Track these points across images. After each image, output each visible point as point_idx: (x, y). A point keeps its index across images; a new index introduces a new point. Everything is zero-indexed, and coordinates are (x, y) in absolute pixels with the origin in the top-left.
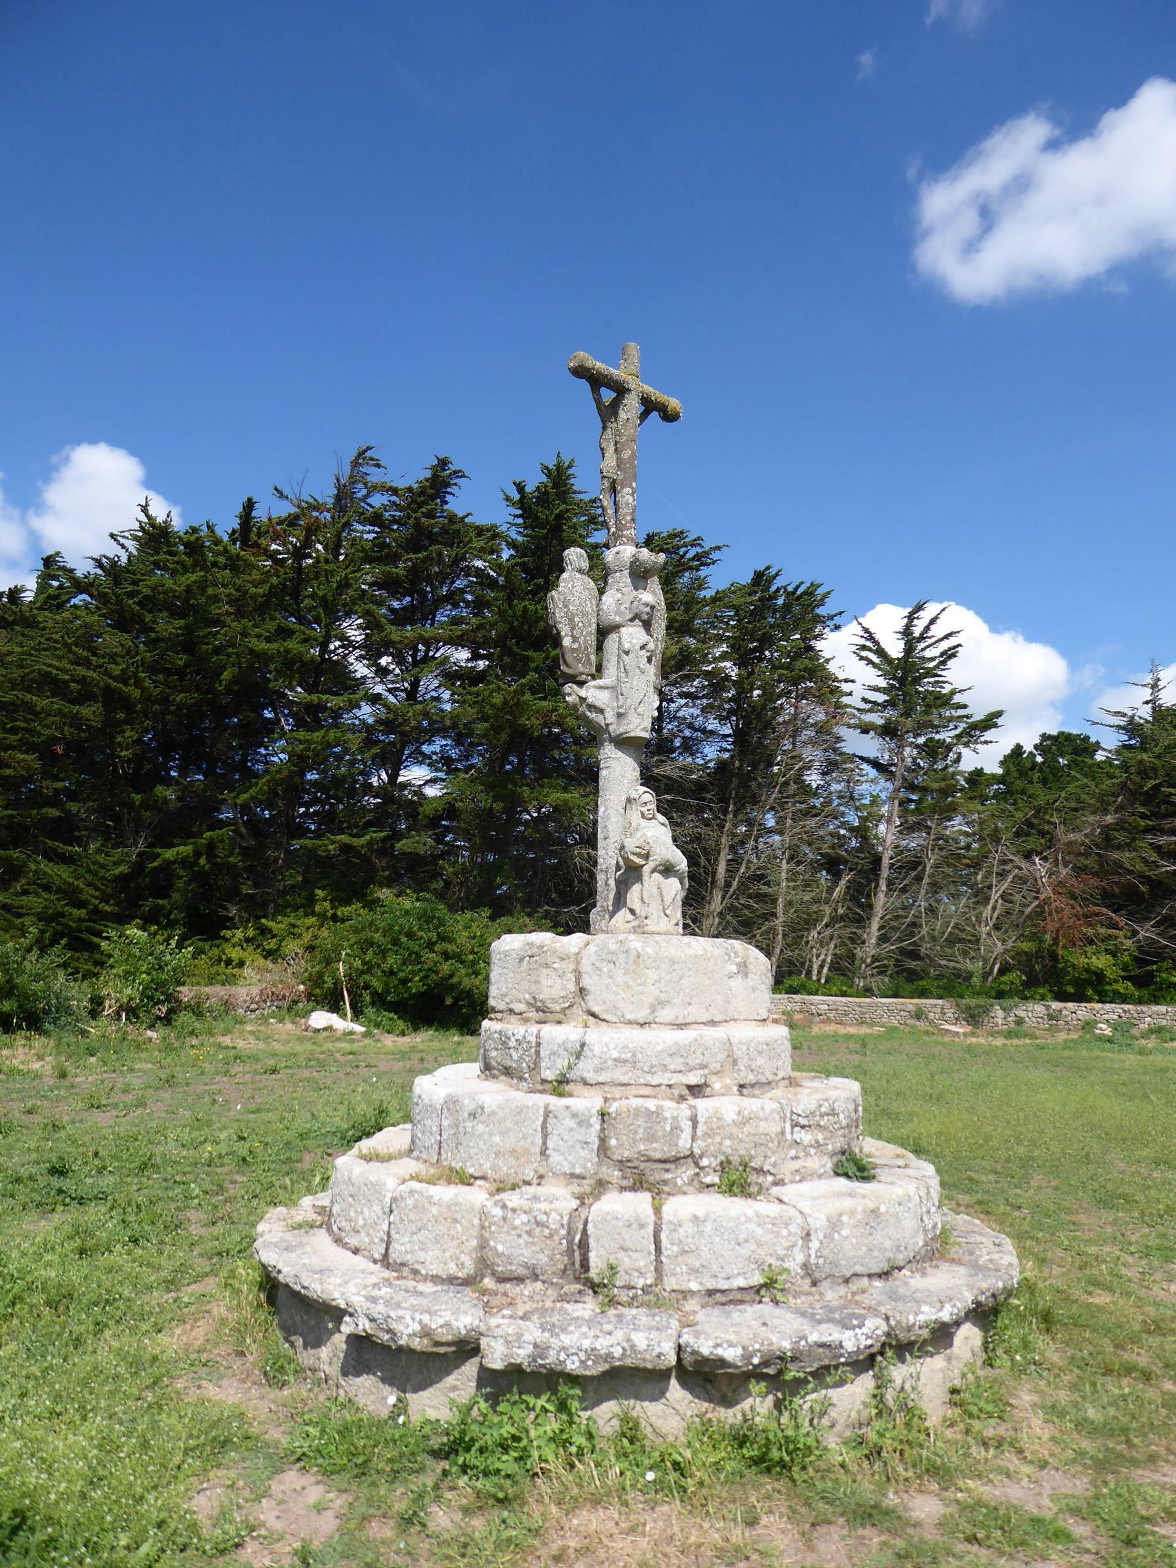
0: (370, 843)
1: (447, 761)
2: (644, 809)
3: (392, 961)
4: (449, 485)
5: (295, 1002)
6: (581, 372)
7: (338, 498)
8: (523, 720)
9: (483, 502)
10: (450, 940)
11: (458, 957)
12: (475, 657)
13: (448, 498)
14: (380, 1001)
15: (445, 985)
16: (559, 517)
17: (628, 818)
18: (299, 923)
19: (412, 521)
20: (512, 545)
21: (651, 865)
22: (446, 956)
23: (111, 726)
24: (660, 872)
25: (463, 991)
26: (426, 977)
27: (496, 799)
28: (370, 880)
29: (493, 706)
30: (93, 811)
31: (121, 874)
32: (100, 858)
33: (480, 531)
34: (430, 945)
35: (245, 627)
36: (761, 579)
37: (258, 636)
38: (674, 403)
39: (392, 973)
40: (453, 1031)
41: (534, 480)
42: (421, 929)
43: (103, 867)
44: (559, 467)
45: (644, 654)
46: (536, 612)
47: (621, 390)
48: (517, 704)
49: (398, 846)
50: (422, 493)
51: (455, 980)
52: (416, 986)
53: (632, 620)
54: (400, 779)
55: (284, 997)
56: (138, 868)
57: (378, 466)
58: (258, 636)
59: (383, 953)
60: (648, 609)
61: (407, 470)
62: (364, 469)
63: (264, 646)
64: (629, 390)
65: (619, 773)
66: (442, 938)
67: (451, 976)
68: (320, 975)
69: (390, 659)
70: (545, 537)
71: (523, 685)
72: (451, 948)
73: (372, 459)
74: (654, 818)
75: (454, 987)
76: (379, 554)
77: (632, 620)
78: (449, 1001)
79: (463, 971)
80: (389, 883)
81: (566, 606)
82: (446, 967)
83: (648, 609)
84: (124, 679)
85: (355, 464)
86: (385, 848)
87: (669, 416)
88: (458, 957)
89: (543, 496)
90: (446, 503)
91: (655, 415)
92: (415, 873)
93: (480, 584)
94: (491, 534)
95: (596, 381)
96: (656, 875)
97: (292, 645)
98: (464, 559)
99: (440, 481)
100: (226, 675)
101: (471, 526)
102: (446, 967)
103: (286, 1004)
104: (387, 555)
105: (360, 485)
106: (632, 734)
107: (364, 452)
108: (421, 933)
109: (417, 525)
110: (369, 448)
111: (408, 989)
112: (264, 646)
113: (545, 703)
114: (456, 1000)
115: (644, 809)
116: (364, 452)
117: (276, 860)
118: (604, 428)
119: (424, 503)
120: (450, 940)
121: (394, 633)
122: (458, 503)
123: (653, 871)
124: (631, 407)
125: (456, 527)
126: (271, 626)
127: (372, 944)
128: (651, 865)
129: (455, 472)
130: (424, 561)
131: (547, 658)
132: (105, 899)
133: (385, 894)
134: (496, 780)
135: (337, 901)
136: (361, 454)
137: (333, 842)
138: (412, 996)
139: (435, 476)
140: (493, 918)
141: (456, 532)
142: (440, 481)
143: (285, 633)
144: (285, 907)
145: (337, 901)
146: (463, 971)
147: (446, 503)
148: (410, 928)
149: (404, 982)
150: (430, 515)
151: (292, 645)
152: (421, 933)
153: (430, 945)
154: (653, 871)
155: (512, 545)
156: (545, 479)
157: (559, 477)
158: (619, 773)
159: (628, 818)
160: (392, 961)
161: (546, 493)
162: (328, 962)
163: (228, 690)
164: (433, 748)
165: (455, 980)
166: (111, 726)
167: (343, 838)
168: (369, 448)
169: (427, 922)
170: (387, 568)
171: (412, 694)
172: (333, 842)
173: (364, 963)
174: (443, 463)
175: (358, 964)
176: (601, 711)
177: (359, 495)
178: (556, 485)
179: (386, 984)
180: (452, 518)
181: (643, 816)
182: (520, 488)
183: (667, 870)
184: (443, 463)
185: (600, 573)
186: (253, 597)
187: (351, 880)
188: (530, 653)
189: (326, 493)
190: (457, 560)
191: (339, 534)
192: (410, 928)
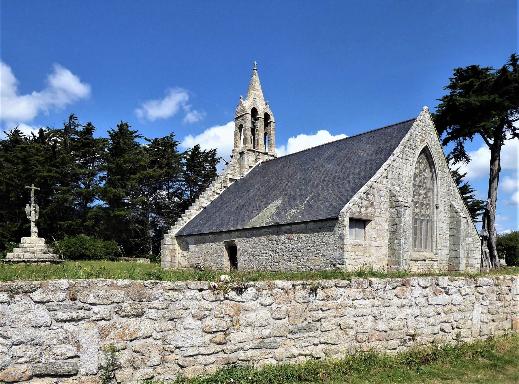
11: (87, 249)
17: (34, 229)
22: (84, 248)
23: (8, 192)
30: (7, 213)
31: (16, 230)
32: (9, 226)
36: (197, 147)
43: (10, 228)
56: (20, 228)
57: (76, 119)
59: (70, 248)
65: (33, 225)
82: (83, 251)
84: (9, 179)
88: (87, 249)
99: (89, 129)
120: (85, 245)
122: (96, 135)
132: (12, 236)
136: (71, 116)
158: (33, 225)
159: (34, 229)
166: (8, 192)
167: (70, 222)
184: (89, 124)
185: (30, 206)
187: (72, 232)
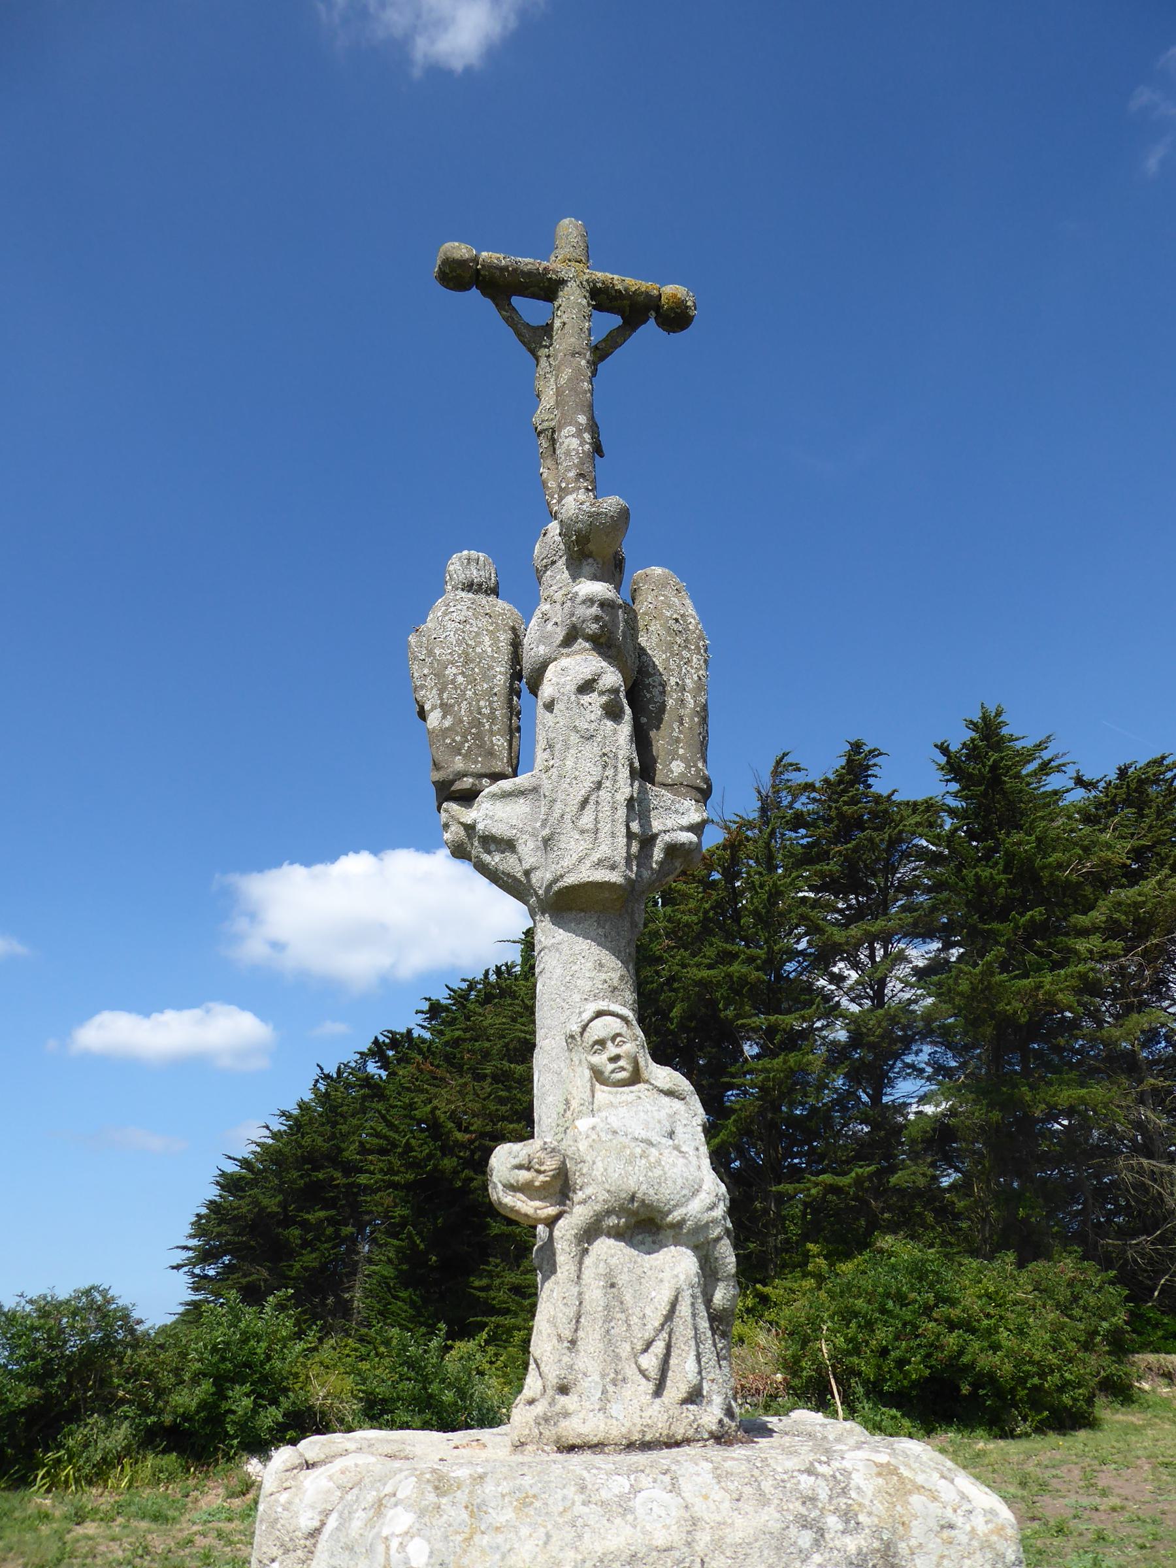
0: (859, 1182)
1: (940, 1069)
2: (600, 1059)
3: (882, 1335)
4: (868, 767)
5: (773, 1397)
6: (457, 276)
7: (763, 810)
8: (1000, 1007)
9: (912, 776)
10: (953, 1302)
12: (948, 946)
13: (871, 781)
14: (877, 1393)
15: (956, 1368)
16: (994, 767)
18: (795, 1286)
19: (833, 813)
20: (952, 812)
21: (578, 1215)
22: (952, 1326)
24: (618, 1234)
25: (981, 1374)
26: (929, 1355)
27: (991, 1106)
28: (874, 1225)
29: (961, 994)
33: (914, 806)
34: (927, 1310)
35: (683, 958)
37: (698, 965)
38: (672, 290)
39: (884, 1352)
40: (980, 1432)
41: (959, 737)
42: (912, 1289)
44: (984, 718)
45: (595, 701)
46: (992, 878)
47: (547, 288)
48: (989, 987)
49: (893, 1180)
50: (840, 782)
51: (965, 1359)
52: (916, 1369)
53: (568, 641)
54: (885, 1099)
55: (758, 1391)
57: (799, 770)
58: (698, 965)
59: (869, 1326)
60: (595, 610)
61: (822, 763)
62: (785, 777)
63: (705, 973)
64: (562, 282)
66: (942, 1299)
67: (961, 1353)
68: (797, 1360)
69: (841, 965)
70: (985, 794)
71: (989, 964)
72: (955, 1313)
73: (791, 765)
74: (636, 1078)
75: (971, 1366)
76: (810, 856)
77: (568, 641)
78: (965, 1389)
79: (976, 1345)
80: (893, 1228)
81: (430, 653)
83: (595, 610)
85: (776, 773)
86: (878, 1185)
87: (676, 319)
89: (973, 752)
90: (870, 786)
91: (650, 328)
92: (917, 1212)
93: (928, 864)
94: (930, 807)
95: (501, 286)
96: (605, 1247)
97: (736, 968)
98: (900, 840)
99: (858, 765)
100: (676, 1012)
101: (899, 805)
102: (952, 1340)
103: (761, 1399)
104: (818, 854)
105: (784, 793)
106: (570, 880)
107: (781, 760)
108: (913, 1295)
109: (841, 815)
110: (785, 755)
111: (906, 1375)
112: (705, 973)
113: (1026, 981)
114: (976, 1386)
115: (600, 1059)
116: (781, 760)
117: (766, 1211)
118: (537, 359)
119: (845, 791)
120: (953, 1302)
121: (839, 936)
123: (589, 1234)
124: (571, 313)
125: (881, 808)
126: (711, 952)
127: (856, 1315)
128: (578, 1215)
129: (870, 752)
130: (855, 850)
131: (1017, 927)
133: (886, 1241)
134: (990, 1088)
135: (833, 1257)
136: (778, 762)
137: (817, 1185)
138: (914, 1384)
139: (850, 761)
140: (1021, 1264)
141: (884, 812)
142: (858, 765)
143: (728, 957)
144: (784, 1266)
145: (833, 1257)
146: (976, 1345)
147: (870, 786)
148: (899, 1290)
149: (901, 1363)
150: (854, 801)
151: (736, 968)
152: (913, 1295)
153: (927, 1310)
154: (589, 1234)
155: (952, 812)
156: (974, 734)
157: (988, 730)
160: (882, 1335)
161: (975, 747)
162: (805, 1342)
163: (682, 1027)
164: (922, 1055)
165: (965, 1359)
167: (826, 1178)
168: (785, 755)
169: (920, 1279)
170: (818, 867)
171: (879, 998)
172: (817, 1185)
173: (849, 1341)
174: (857, 747)
175: (840, 1341)
176: (508, 845)
177: (785, 803)
178: (985, 737)
179: (879, 1367)
180: (878, 799)
181: (598, 1075)
182: (944, 749)
183: (643, 1224)
186: (687, 925)
188: (995, 925)
189: (752, 812)
190: (893, 843)
191: (768, 844)
192: (899, 1290)
